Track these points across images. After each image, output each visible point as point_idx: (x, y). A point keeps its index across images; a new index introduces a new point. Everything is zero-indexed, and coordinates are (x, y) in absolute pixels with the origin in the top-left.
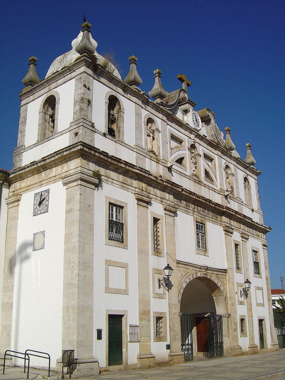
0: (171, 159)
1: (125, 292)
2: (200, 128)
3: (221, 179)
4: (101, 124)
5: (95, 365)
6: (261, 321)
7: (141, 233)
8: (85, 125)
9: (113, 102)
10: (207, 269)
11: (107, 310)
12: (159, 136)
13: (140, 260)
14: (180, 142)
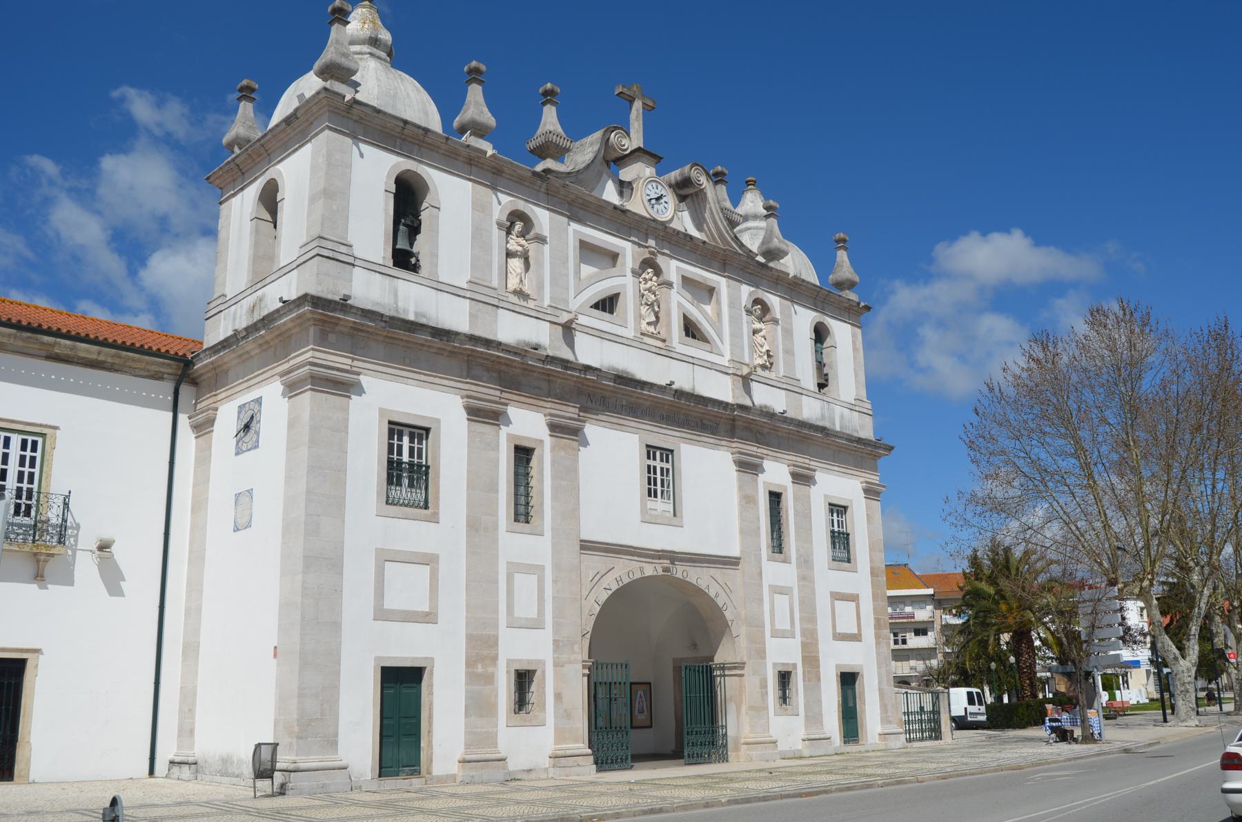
0: (579, 301)
1: (429, 617)
2: (670, 217)
3: (736, 335)
4: (809, 380)
5: (340, 777)
6: (848, 680)
7: (479, 485)
8: (325, 253)
9: (820, 334)
10: (673, 557)
11: (837, 666)
12: (543, 255)
13: (472, 549)
14: (613, 257)
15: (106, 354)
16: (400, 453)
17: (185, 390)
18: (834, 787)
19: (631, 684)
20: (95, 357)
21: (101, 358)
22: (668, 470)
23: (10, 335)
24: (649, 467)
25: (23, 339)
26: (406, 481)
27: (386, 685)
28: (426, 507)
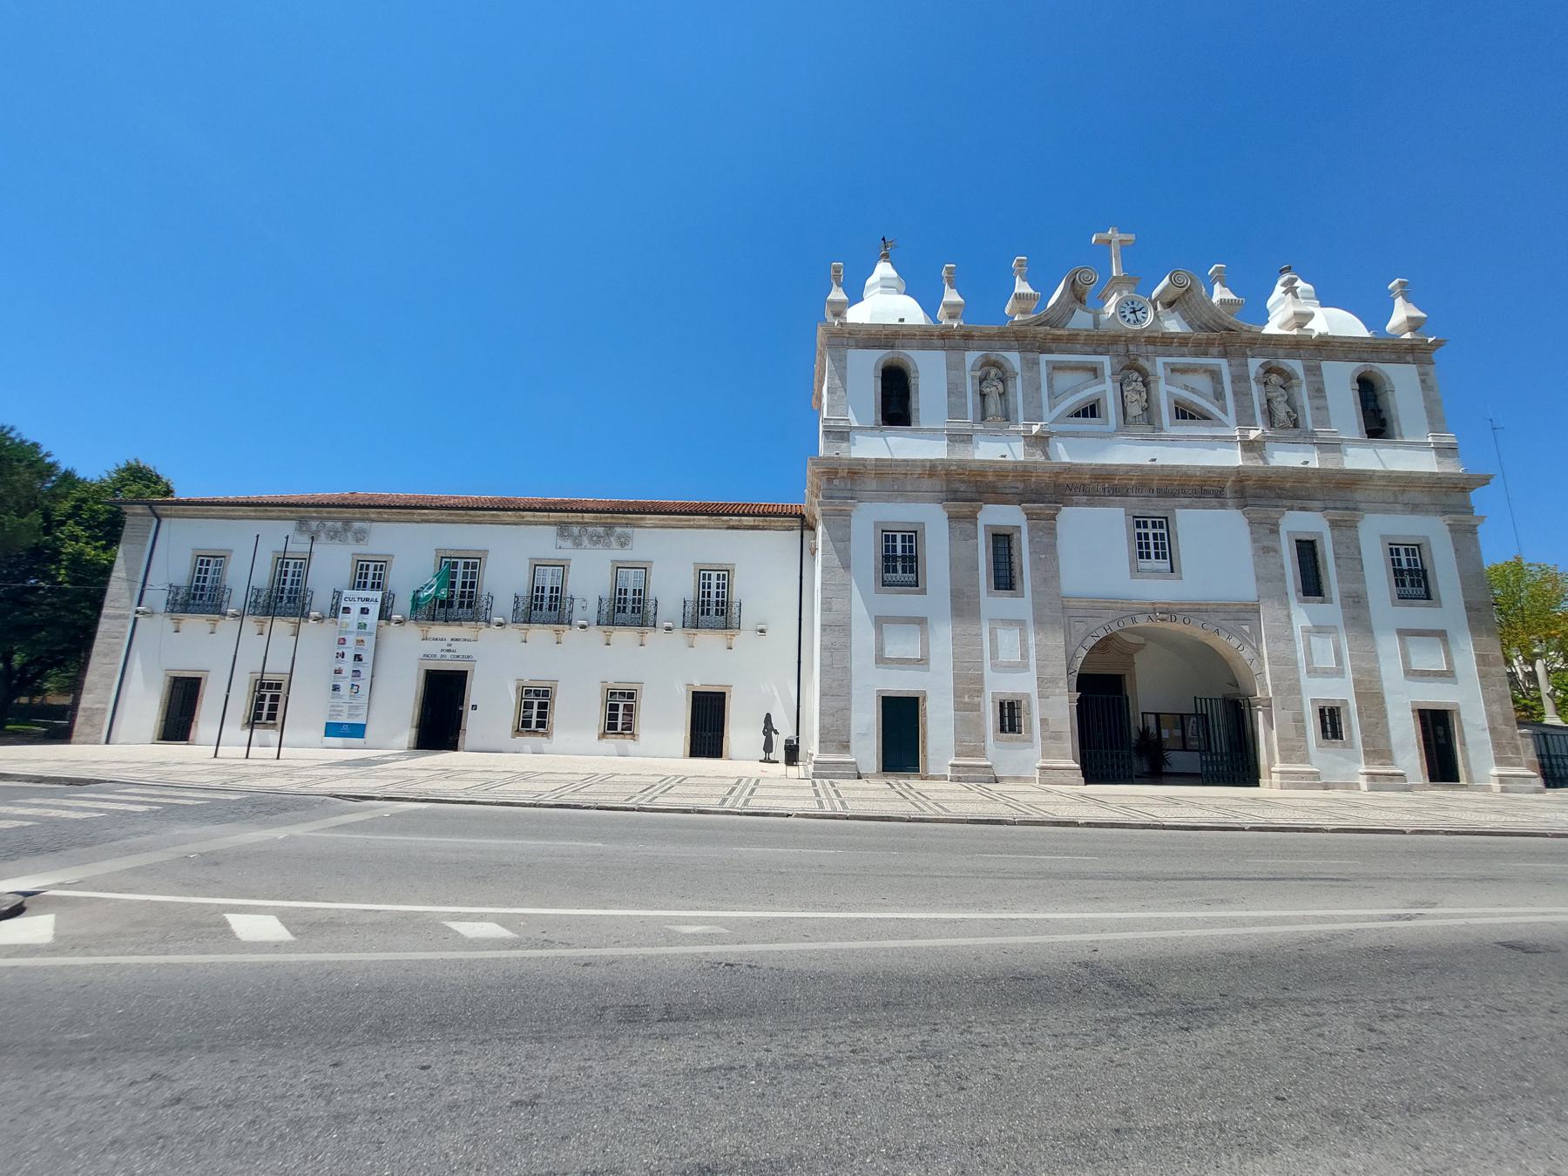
7: (961, 567)
15: (758, 521)
16: (1400, 564)
17: (806, 533)
18: (1250, 825)
19: (1143, 713)
20: (753, 524)
21: (756, 523)
22: (1162, 535)
23: (706, 520)
24: (1139, 534)
25: (713, 520)
26: (899, 568)
27: (1428, 715)
28: (917, 586)
